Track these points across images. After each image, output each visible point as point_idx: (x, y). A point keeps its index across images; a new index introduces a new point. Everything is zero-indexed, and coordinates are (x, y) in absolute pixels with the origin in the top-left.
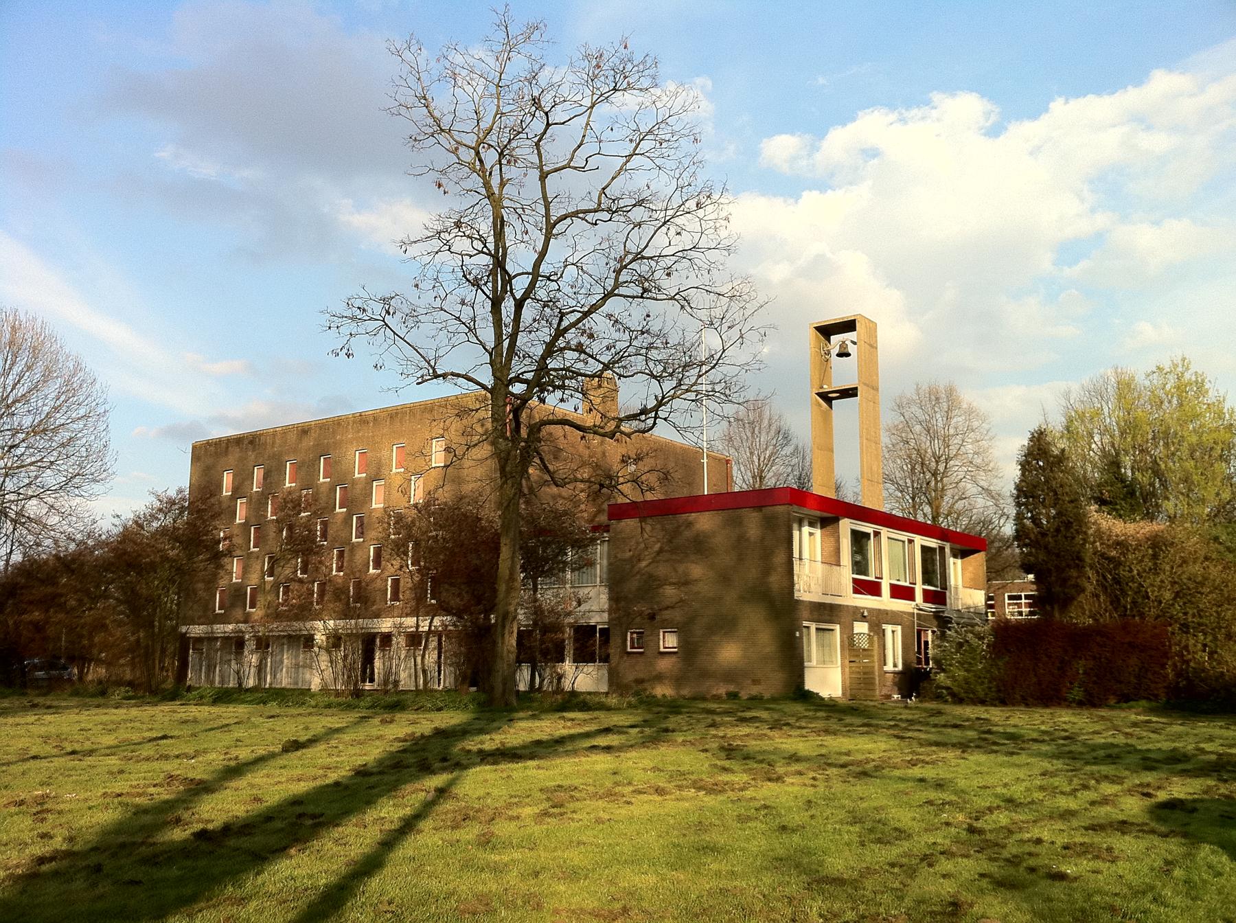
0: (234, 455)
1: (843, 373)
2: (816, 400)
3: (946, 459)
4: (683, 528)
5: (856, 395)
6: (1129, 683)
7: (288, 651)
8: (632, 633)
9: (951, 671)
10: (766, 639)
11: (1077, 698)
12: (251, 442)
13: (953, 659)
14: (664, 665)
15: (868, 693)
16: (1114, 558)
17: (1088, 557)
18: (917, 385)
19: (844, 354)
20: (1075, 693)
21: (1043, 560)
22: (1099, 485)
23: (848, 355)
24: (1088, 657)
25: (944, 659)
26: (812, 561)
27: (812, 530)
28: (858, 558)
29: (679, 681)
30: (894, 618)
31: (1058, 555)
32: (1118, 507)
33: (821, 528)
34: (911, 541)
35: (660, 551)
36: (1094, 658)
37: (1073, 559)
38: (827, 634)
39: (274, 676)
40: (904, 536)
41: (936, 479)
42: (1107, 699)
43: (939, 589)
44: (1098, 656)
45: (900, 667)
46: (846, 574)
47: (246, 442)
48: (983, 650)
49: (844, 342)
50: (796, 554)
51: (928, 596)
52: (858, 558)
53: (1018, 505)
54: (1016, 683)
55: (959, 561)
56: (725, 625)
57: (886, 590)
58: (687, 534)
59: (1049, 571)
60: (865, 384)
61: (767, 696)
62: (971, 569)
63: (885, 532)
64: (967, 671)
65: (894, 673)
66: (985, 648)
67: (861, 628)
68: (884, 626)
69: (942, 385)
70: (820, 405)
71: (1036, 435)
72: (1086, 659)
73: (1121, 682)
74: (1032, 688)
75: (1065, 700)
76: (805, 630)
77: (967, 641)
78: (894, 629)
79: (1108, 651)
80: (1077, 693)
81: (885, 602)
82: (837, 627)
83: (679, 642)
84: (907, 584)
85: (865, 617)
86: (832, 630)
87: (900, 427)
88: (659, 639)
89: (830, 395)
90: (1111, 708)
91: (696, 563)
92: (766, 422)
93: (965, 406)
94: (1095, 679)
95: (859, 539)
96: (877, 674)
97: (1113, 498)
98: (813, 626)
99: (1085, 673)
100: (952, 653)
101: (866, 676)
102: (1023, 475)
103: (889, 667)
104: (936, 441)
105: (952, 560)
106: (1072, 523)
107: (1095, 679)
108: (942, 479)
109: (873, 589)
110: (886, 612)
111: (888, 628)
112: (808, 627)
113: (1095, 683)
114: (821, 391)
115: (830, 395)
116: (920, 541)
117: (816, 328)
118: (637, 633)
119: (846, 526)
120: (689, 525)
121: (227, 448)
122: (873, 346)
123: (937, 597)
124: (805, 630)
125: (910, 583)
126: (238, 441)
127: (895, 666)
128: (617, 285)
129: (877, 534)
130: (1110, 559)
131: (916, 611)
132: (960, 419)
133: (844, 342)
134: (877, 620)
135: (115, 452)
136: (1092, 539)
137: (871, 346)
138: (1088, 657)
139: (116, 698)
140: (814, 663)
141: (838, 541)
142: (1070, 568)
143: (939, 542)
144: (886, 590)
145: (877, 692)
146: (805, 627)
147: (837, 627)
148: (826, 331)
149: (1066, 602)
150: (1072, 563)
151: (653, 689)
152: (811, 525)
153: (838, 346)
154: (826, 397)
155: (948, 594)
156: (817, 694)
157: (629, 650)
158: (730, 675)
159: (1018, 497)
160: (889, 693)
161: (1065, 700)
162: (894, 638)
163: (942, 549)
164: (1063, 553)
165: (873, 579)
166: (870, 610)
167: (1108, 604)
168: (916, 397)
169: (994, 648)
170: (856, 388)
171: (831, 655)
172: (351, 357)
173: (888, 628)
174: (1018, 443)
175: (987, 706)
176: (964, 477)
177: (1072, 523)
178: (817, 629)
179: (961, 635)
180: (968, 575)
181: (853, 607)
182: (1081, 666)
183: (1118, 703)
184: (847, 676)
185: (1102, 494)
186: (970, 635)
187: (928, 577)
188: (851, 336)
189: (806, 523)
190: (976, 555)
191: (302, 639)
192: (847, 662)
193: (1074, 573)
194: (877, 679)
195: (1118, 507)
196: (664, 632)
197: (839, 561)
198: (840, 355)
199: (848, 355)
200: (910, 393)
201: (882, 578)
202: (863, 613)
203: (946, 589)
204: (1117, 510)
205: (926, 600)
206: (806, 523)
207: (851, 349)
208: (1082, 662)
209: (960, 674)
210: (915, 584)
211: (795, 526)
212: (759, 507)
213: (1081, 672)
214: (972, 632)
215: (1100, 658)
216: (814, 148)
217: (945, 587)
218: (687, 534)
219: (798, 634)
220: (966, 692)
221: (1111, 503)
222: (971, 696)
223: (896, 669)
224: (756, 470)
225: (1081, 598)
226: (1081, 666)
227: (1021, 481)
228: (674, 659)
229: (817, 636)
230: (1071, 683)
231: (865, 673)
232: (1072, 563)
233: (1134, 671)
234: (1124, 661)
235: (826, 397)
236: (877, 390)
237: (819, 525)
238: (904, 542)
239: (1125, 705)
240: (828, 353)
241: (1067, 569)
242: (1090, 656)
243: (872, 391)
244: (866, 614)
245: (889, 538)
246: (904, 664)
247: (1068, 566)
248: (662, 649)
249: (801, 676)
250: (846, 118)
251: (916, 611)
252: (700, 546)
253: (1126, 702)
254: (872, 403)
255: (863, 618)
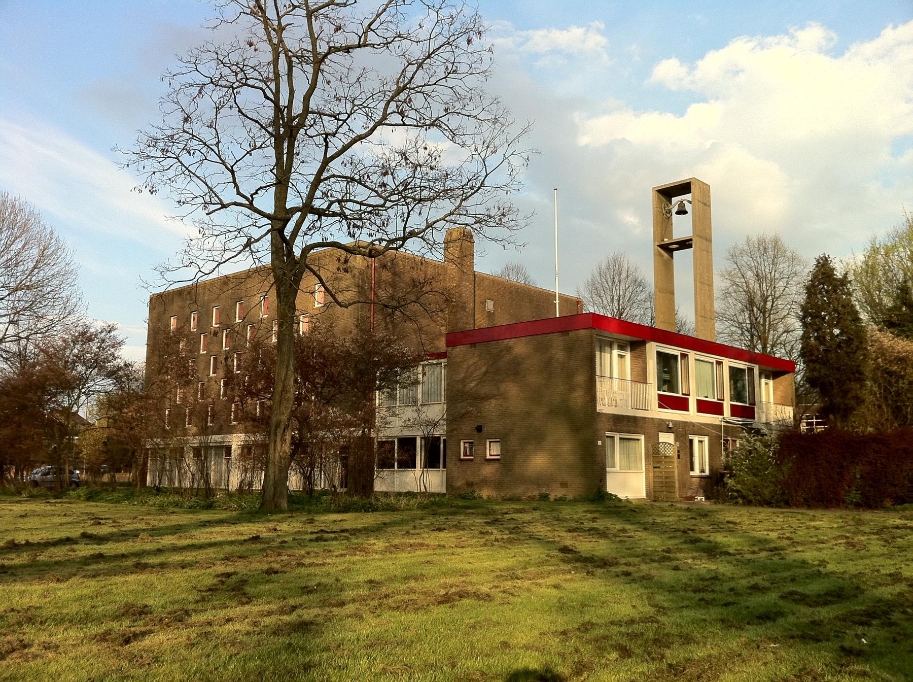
0: (177, 303)
1: (682, 228)
2: (658, 251)
3: (773, 300)
4: (504, 352)
5: (690, 246)
6: (903, 486)
7: (215, 458)
8: (465, 443)
9: (740, 475)
10: (567, 448)
11: (854, 500)
12: (189, 293)
13: (742, 465)
14: (488, 471)
15: (669, 495)
16: (895, 372)
17: (868, 372)
18: (748, 238)
19: (682, 212)
20: (852, 495)
21: (825, 374)
22: (890, 310)
23: (685, 212)
24: (864, 463)
25: (736, 465)
26: (622, 379)
27: (767, 381)
28: (667, 377)
29: (498, 485)
30: (700, 429)
31: (838, 369)
32: (905, 329)
33: (631, 351)
34: (719, 363)
35: (487, 372)
36: (871, 463)
37: (853, 374)
38: (632, 443)
39: (180, 482)
40: (713, 358)
41: (764, 315)
42: (882, 501)
43: (747, 405)
44: (874, 461)
45: (707, 473)
46: (653, 391)
47: (185, 293)
48: (770, 457)
49: (682, 202)
50: (598, 373)
51: (735, 411)
52: (667, 377)
53: (805, 325)
54: (798, 486)
55: (771, 382)
56: (535, 438)
57: (693, 405)
58: (507, 358)
59: (831, 384)
60: (699, 236)
61: (570, 497)
62: (781, 388)
63: (692, 355)
64: (755, 475)
65: (701, 477)
66: (771, 454)
67: (667, 438)
68: (691, 437)
69: (769, 235)
70: (661, 255)
71: (820, 261)
72: (863, 465)
73: (895, 486)
74: (813, 491)
75: (844, 502)
76: (608, 441)
77: (755, 449)
78: (700, 439)
79: (883, 457)
80: (855, 496)
81: (692, 415)
82: (642, 437)
83: (501, 450)
84: (715, 400)
85: (670, 428)
86: (638, 440)
87: (733, 273)
88: (486, 448)
89: (671, 247)
90: (887, 509)
91: (503, 382)
92: (624, 275)
93: (789, 254)
94: (871, 482)
95: (666, 361)
96: (677, 478)
97: (901, 321)
98: (617, 436)
99: (862, 477)
100: (742, 459)
101: (667, 480)
102: (808, 298)
103: (697, 472)
104: (764, 284)
105: (763, 381)
106: (853, 340)
107: (871, 482)
108: (769, 316)
109: (681, 404)
110: (693, 424)
111: (696, 439)
112: (612, 437)
113: (871, 486)
114: (662, 243)
115: (677, 246)
116: (727, 362)
117: (659, 191)
118: (470, 443)
119: (653, 348)
120: (509, 349)
121: (173, 298)
122: (707, 204)
123: (746, 412)
124: (608, 441)
125: (718, 400)
126: (180, 292)
127: (703, 471)
128: (385, 116)
129: (684, 356)
130: (890, 373)
131: (723, 424)
132: (785, 265)
133: (682, 202)
134: (683, 432)
135: (87, 303)
136: (874, 355)
137: (705, 205)
138: (864, 463)
139: (25, 495)
140: (617, 468)
141: (645, 362)
142: (851, 381)
143: (747, 364)
144: (693, 405)
145: (677, 495)
146: (607, 437)
147: (642, 437)
148: (667, 193)
149: (846, 412)
150: (852, 376)
151: (480, 490)
152: (621, 347)
153: (677, 206)
154: (665, 247)
155: (756, 409)
156: (616, 496)
157: (462, 457)
158: (539, 481)
159: (804, 317)
160: (694, 495)
161: (844, 502)
162: (701, 448)
163: (751, 370)
164: (843, 367)
165: (680, 395)
166: (676, 423)
167: (890, 414)
168: (746, 248)
169: (779, 456)
170: (691, 240)
171: (636, 461)
172: (154, 193)
173: (696, 439)
174: (807, 269)
175: (772, 507)
176: (788, 314)
177: (853, 340)
178: (621, 439)
179: (750, 443)
180: (779, 393)
181: (659, 419)
182: (857, 471)
183: (893, 505)
184: (651, 480)
185: (891, 317)
186: (758, 443)
187: (737, 395)
188: (688, 197)
189: (615, 346)
190: (786, 376)
191: (224, 450)
192: (651, 467)
193: (854, 385)
194: (677, 482)
195: (905, 329)
196: (490, 442)
197: (646, 379)
198: (678, 213)
199: (685, 212)
200: (742, 244)
201: (689, 395)
202: (668, 425)
203: (755, 405)
204: (904, 331)
205: (733, 415)
206: (615, 346)
207: (688, 207)
208: (859, 468)
209: (748, 478)
210: (723, 400)
211: (597, 349)
212: (565, 332)
213: (858, 476)
214: (760, 441)
215: (876, 464)
216: (692, 68)
217: (753, 403)
218: (507, 358)
219: (600, 443)
220: (754, 495)
221: (899, 325)
222: (758, 498)
223: (703, 474)
224: (615, 311)
225: (863, 409)
226: (857, 471)
227: (807, 303)
228: (497, 465)
229: (620, 442)
230: (849, 487)
231: (666, 478)
232: (852, 376)
233: (908, 475)
234: (898, 466)
235: (665, 247)
236: (710, 241)
237: (629, 349)
238: (712, 363)
239: (899, 507)
240: (670, 212)
241: (848, 382)
242: (867, 461)
243: (704, 241)
244: (671, 425)
245: (696, 360)
246: (710, 470)
247: (850, 380)
248: (488, 457)
249: (601, 478)
250: (719, 44)
251: (723, 424)
252: (515, 370)
253: (899, 504)
254: (705, 252)
255: (669, 430)
